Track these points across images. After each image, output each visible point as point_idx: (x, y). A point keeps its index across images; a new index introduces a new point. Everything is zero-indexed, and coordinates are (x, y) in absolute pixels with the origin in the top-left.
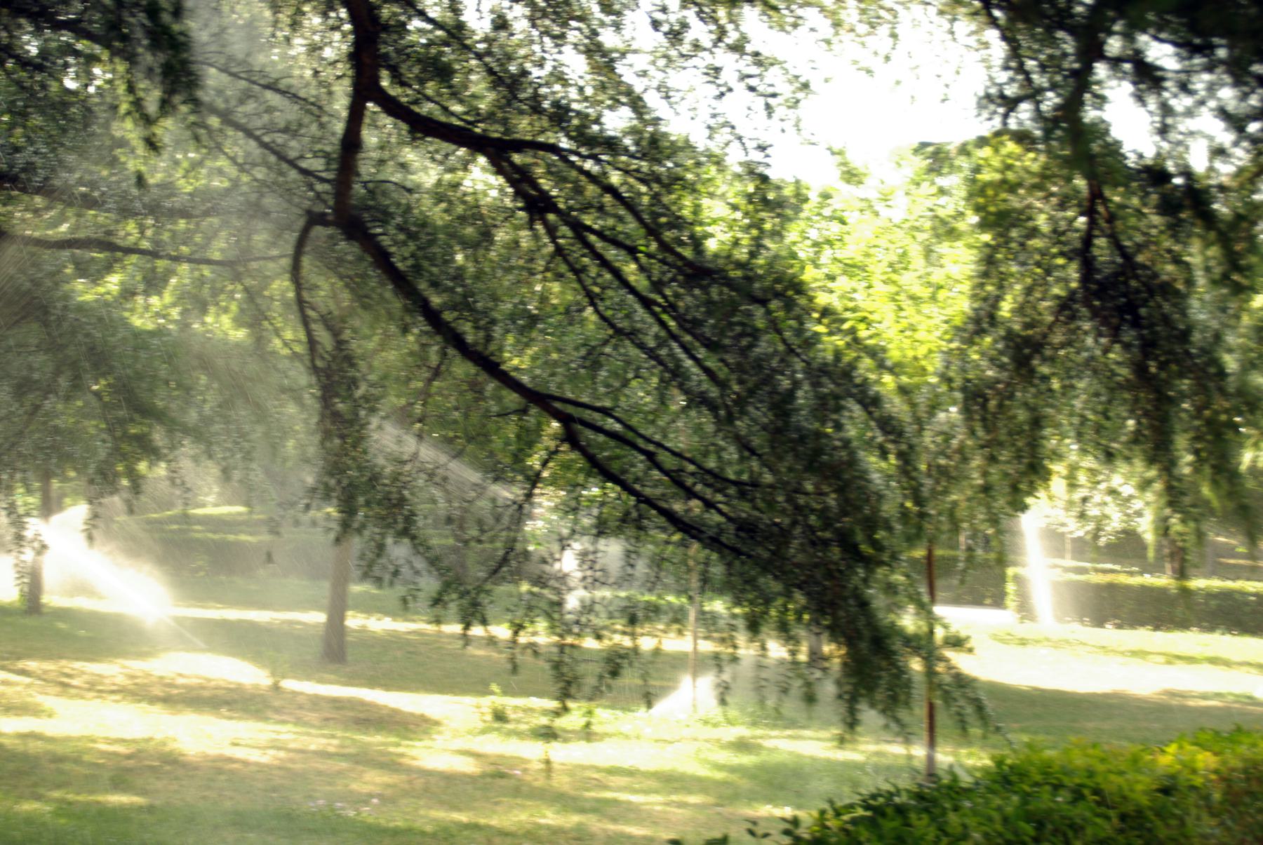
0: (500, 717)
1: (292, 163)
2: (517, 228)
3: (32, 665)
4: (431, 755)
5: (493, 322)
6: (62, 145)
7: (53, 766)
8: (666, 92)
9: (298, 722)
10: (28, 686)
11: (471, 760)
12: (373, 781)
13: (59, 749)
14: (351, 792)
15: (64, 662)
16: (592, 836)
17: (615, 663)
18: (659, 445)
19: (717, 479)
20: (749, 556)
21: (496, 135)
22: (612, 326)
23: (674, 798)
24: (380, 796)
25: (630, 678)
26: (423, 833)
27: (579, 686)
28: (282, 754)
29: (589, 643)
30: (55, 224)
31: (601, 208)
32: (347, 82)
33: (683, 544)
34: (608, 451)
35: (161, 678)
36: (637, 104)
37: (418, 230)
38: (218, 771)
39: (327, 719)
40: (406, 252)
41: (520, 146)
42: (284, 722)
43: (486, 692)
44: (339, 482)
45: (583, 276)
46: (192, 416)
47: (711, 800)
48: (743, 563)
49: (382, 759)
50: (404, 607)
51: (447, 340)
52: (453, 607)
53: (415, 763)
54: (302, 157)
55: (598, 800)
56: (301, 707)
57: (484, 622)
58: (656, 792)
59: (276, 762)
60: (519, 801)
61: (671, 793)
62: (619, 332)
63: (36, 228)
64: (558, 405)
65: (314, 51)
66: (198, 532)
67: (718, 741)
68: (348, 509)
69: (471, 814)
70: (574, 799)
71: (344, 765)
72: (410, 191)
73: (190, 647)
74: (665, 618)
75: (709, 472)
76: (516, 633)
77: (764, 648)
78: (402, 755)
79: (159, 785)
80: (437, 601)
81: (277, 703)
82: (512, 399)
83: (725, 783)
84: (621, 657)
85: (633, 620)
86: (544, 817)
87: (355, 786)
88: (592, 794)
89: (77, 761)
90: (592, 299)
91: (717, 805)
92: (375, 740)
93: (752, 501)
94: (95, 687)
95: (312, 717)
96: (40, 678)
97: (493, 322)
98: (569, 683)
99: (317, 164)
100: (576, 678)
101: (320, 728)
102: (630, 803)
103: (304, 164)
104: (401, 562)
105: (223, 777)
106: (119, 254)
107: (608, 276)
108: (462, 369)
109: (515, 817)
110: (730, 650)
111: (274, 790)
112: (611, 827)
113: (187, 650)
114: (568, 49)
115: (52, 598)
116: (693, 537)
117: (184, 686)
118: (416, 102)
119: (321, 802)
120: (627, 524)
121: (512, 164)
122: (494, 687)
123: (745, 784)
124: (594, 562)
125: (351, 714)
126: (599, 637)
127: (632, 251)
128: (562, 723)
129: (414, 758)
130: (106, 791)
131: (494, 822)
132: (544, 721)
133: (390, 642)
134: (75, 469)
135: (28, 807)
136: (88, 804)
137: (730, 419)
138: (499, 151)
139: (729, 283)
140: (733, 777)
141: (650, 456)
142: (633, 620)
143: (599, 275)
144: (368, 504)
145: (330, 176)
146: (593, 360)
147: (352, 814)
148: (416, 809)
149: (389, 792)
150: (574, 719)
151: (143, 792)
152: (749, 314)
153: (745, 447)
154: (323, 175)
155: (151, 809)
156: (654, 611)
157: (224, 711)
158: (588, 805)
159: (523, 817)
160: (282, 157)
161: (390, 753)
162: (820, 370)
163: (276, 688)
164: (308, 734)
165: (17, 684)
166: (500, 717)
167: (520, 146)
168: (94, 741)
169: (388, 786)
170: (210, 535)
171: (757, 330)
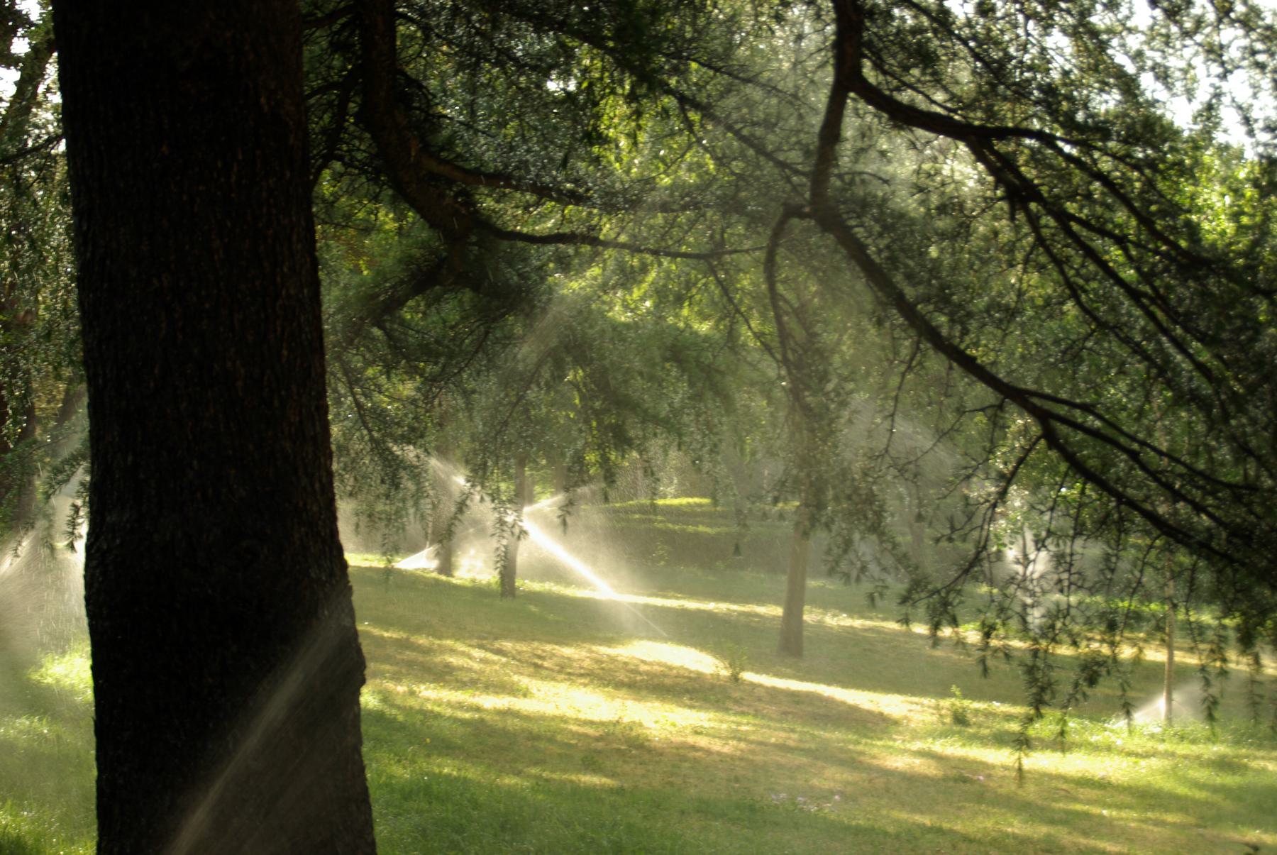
0: (960, 719)
1: (769, 156)
2: (996, 218)
3: (508, 645)
4: (898, 757)
5: (970, 315)
6: (552, 142)
7: (529, 743)
8: (1163, 76)
9: (757, 714)
10: (504, 665)
11: (932, 763)
12: (832, 777)
13: (535, 728)
14: (812, 788)
15: (536, 644)
16: (1062, 849)
17: (1092, 671)
18: (1143, 443)
19: (1210, 482)
20: (1243, 564)
21: (977, 123)
22: (1096, 319)
23: (1150, 815)
24: (841, 793)
25: (1105, 688)
26: (886, 834)
27: (1053, 693)
28: (743, 745)
29: (1065, 650)
30: (543, 217)
31: (1088, 196)
32: (830, 69)
33: (1167, 549)
34: (1089, 453)
35: (626, 663)
36: (1129, 86)
37: (893, 222)
38: (680, 757)
39: (785, 713)
40: (883, 243)
41: (1004, 133)
42: (743, 714)
43: (946, 694)
44: (809, 476)
45: (1066, 268)
46: (664, 410)
47: (1191, 820)
48: (1235, 571)
49: (843, 756)
50: (871, 604)
51: (920, 334)
52: (921, 610)
53: (875, 762)
54: (779, 149)
55: (1068, 812)
56: (760, 699)
57: (954, 622)
58: (1130, 807)
59: (738, 753)
60: (983, 807)
61: (1146, 810)
62: (1102, 325)
63: (525, 223)
64: (1036, 401)
65: (795, 45)
66: (660, 523)
67: (1198, 757)
68: (815, 505)
69: (935, 817)
70: (1042, 809)
71: (804, 760)
72: (886, 182)
73: (654, 637)
74: (1146, 626)
75: (1201, 473)
76: (987, 635)
77: (1257, 661)
78: (862, 753)
79: (627, 768)
80: (905, 600)
81: (737, 695)
82: (980, 392)
83: (1206, 803)
84: (1099, 664)
85: (1112, 627)
86: (1011, 825)
87: (815, 782)
88: (1061, 805)
89: (551, 740)
90: (1074, 292)
91: (1198, 826)
92: (835, 736)
93: (1248, 505)
94: (565, 671)
95: (772, 709)
96: (514, 658)
97: (970, 315)
98: (1043, 689)
99: (795, 156)
100: (1050, 684)
101: (780, 721)
102: (1102, 817)
103: (781, 157)
104: (868, 558)
105: (687, 765)
106: (600, 248)
107: (1092, 267)
108: (936, 363)
109: (982, 823)
110: (1218, 664)
111: (737, 780)
112: (1082, 841)
113: (649, 639)
114: (1055, 31)
115: (526, 584)
116: (1178, 541)
117: (647, 673)
118: (898, 89)
119: (783, 795)
120: (1110, 526)
121: (996, 153)
122: (954, 689)
123: (1228, 805)
124: (1071, 565)
125: (809, 709)
126: (1075, 644)
127: (1121, 241)
128: (1032, 731)
129: (874, 757)
130: (579, 771)
131: (958, 827)
132: (1015, 727)
133: (848, 638)
134: (548, 457)
135: (509, 781)
136: (563, 782)
137: (1226, 417)
138: (981, 140)
139: (1232, 275)
140: (1217, 798)
141: (1134, 455)
142: (1112, 627)
143: (1083, 266)
144: (836, 499)
145: (807, 169)
146: (1073, 354)
147: (814, 809)
148: (878, 809)
149: (849, 789)
150: (1044, 728)
151: (613, 775)
152: (1252, 307)
153: (1243, 451)
154: (800, 167)
155: (620, 792)
156: (1134, 619)
157: (686, 699)
158: (1057, 817)
159: (989, 824)
160: (761, 150)
161: (850, 750)
162: (818, 350)
163: (735, 678)
164: (769, 727)
165: (494, 663)
166: (960, 719)
167: (1004, 133)
168: (566, 722)
169: (849, 783)
170: (670, 526)
171: (1260, 324)
